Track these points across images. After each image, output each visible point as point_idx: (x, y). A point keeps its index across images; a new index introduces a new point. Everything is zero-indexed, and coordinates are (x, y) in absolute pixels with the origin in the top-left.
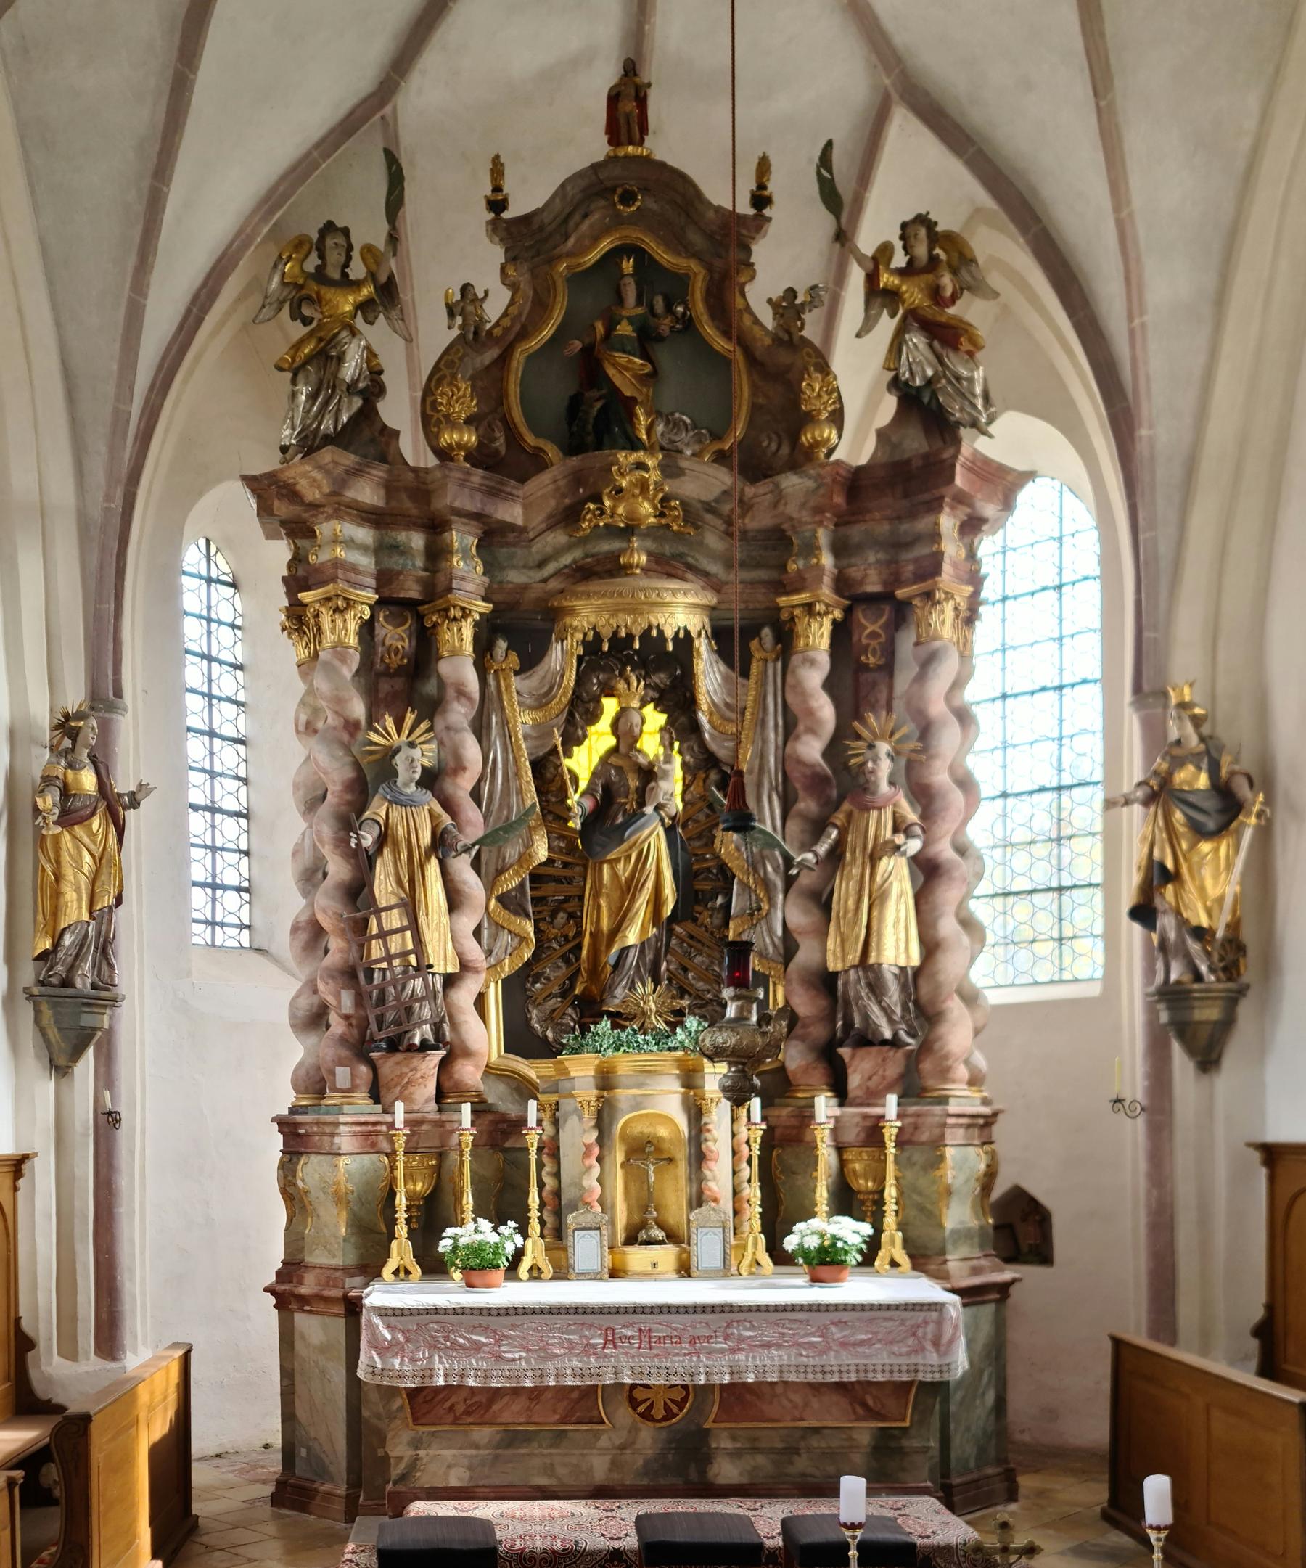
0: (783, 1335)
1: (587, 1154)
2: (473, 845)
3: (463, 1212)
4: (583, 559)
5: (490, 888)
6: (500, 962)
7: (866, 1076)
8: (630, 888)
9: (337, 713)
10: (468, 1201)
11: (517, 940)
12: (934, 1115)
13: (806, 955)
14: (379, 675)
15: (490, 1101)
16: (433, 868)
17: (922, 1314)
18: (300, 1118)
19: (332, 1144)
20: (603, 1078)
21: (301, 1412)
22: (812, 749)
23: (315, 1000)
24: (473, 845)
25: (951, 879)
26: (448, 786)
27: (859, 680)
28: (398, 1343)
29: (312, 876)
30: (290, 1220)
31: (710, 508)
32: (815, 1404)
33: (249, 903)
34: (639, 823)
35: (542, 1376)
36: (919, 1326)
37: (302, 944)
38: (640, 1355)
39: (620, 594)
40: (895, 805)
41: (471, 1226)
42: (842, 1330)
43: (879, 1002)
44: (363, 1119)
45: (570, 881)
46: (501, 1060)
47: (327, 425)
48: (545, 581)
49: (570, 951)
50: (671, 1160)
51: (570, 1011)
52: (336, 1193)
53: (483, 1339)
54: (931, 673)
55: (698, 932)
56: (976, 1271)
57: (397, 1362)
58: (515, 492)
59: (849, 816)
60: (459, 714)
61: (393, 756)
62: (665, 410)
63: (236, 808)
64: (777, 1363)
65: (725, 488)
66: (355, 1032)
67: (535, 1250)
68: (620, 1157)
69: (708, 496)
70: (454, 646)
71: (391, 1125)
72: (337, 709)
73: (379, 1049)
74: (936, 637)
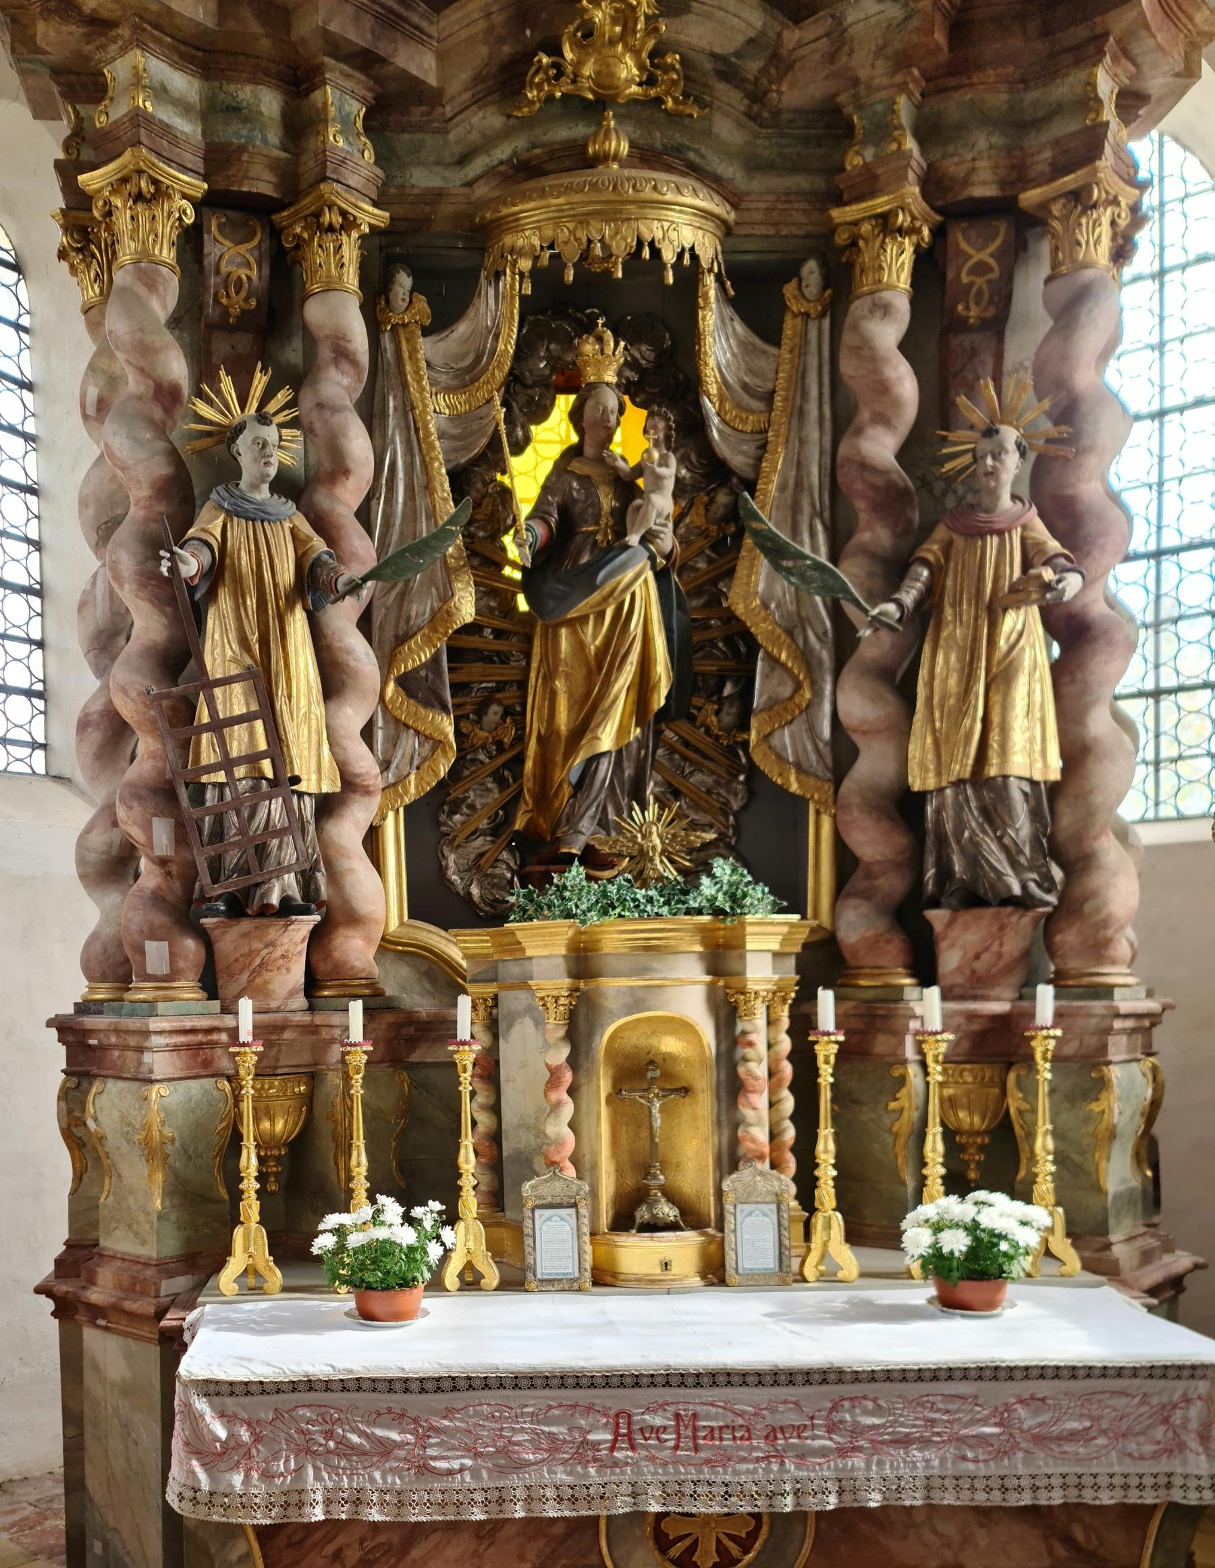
0: (933, 1422)
1: (553, 1080)
2: (365, 579)
3: (350, 1178)
4: (528, 150)
5: (387, 662)
6: (402, 780)
7: (971, 954)
8: (602, 666)
9: (142, 371)
10: (360, 1163)
11: (427, 746)
12: (1090, 1015)
13: (872, 765)
14: (212, 327)
15: (389, 992)
16: (298, 623)
18: (90, 1021)
19: (140, 1063)
20: (577, 958)
21: (94, 1483)
22: (881, 446)
23: (115, 836)
24: (365, 579)
25: (1110, 643)
26: (322, 499)
27: (954, 335)
28: (240, 1445)
29: (106, 641)
30: (78, 1178)
31: (727, 70)
32: (982, 1538)
33: (44, 713)
34: (617, 561)
35: (501, 1501)
36: (1174, 1407)
37: (94, 748)
38: (677, 1462)
39: (594, 187)
41: (367, 1211)
42: (1036, 1412)
44: (188, 1024)
45: (504, 658)
46: (404, 930)
48: (469, 184)
49: (505, 765)
50: (686, 1091)
51: (505, 855)
52: (147, 1142)
53: (395, 1436)
55: (697, 736)
57: (237, 1480)
58: (424, 25)
59: (947, 548)
60: (339, 386)
61: (233, 439)
63: (24, 581)
64: (921, 1472)
66: (177, 885)
67: (466, 1240)
68: (604, 1086)
69: (727, 44)
70: (329, 276)
71: (234, 1032)
72: (142, 363)
73: (214, 913)
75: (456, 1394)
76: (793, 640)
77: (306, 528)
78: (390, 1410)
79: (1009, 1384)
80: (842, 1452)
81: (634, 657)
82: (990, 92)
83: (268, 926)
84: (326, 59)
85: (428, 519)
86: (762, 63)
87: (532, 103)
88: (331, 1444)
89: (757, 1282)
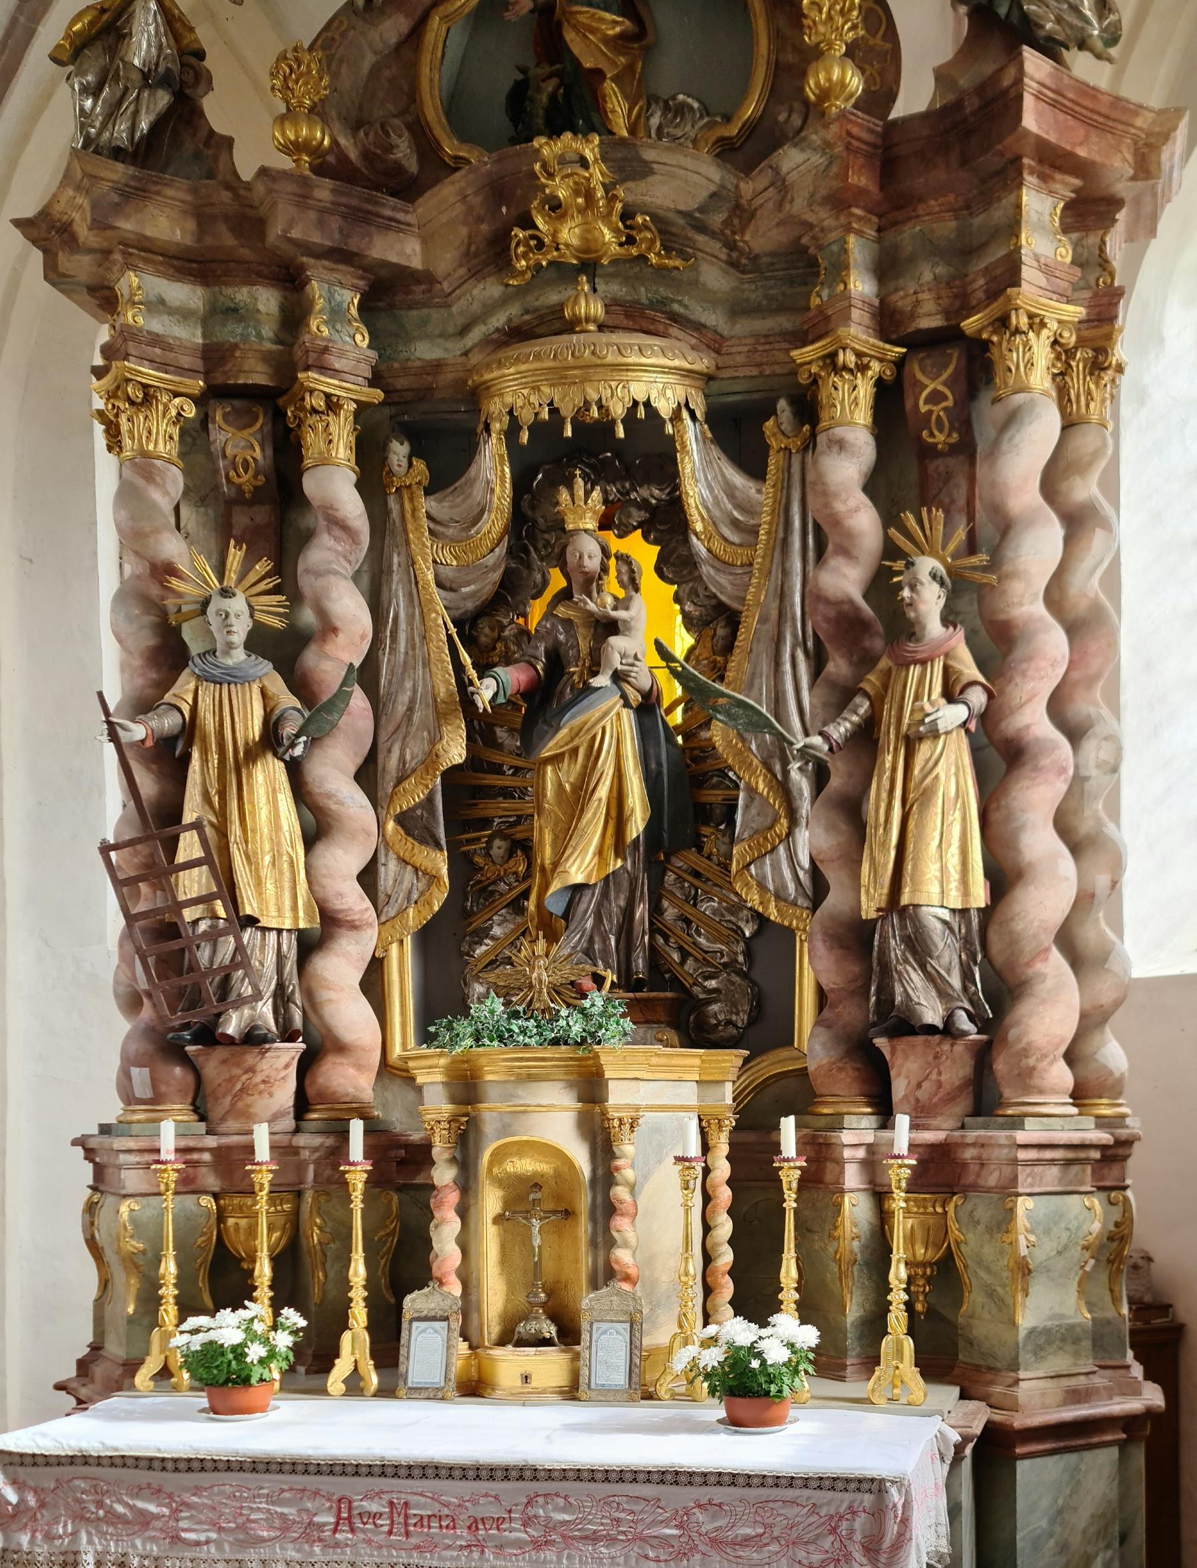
0: (618, 1520)
9: (137, 553)
11: (424, 881)
14: (230, 503)
17: (848, 1497)
22: (846, 580)
26: (311, 658)
28: (29, 1509)
38: (391, 1546)
40: (947, 655)
42: (714, 1517)
43: (923, 966)
47: (120, 131)
53: (153, 1508)
54: (1005, 446)
55: (701, 864)
56: (1076, 1396)
58: (400, 216)
62: (664, 93)
65: (713, 188)
69: (689, 203)
74: (1024, 389)
75: (203, 1475)
76: (770, 770)
77: (277, 685)
78: (149, 1486)
79: (689, 1488)
80: (538, 1545)
81: (603, 792)
82: (936, 222)
83: (244, 1053)
84: (304, 259)
85: (424, 666)
86: (726, 215)
87: (523, 273)
88: (101, 1513)
89: (608, 1396)
